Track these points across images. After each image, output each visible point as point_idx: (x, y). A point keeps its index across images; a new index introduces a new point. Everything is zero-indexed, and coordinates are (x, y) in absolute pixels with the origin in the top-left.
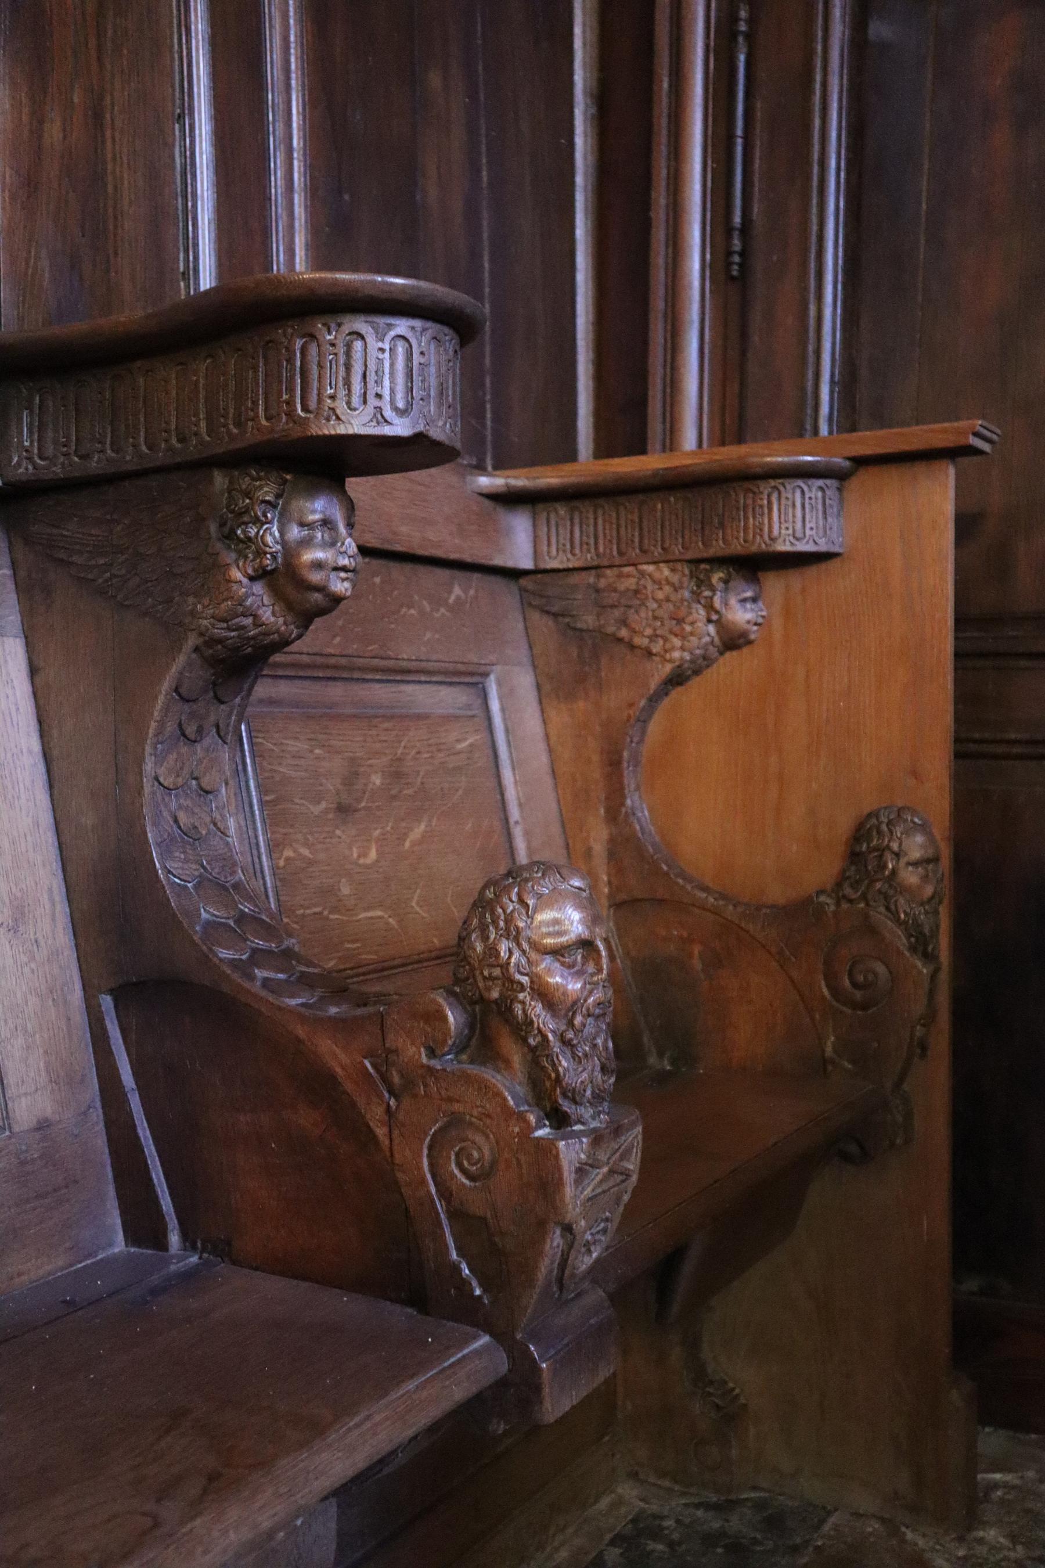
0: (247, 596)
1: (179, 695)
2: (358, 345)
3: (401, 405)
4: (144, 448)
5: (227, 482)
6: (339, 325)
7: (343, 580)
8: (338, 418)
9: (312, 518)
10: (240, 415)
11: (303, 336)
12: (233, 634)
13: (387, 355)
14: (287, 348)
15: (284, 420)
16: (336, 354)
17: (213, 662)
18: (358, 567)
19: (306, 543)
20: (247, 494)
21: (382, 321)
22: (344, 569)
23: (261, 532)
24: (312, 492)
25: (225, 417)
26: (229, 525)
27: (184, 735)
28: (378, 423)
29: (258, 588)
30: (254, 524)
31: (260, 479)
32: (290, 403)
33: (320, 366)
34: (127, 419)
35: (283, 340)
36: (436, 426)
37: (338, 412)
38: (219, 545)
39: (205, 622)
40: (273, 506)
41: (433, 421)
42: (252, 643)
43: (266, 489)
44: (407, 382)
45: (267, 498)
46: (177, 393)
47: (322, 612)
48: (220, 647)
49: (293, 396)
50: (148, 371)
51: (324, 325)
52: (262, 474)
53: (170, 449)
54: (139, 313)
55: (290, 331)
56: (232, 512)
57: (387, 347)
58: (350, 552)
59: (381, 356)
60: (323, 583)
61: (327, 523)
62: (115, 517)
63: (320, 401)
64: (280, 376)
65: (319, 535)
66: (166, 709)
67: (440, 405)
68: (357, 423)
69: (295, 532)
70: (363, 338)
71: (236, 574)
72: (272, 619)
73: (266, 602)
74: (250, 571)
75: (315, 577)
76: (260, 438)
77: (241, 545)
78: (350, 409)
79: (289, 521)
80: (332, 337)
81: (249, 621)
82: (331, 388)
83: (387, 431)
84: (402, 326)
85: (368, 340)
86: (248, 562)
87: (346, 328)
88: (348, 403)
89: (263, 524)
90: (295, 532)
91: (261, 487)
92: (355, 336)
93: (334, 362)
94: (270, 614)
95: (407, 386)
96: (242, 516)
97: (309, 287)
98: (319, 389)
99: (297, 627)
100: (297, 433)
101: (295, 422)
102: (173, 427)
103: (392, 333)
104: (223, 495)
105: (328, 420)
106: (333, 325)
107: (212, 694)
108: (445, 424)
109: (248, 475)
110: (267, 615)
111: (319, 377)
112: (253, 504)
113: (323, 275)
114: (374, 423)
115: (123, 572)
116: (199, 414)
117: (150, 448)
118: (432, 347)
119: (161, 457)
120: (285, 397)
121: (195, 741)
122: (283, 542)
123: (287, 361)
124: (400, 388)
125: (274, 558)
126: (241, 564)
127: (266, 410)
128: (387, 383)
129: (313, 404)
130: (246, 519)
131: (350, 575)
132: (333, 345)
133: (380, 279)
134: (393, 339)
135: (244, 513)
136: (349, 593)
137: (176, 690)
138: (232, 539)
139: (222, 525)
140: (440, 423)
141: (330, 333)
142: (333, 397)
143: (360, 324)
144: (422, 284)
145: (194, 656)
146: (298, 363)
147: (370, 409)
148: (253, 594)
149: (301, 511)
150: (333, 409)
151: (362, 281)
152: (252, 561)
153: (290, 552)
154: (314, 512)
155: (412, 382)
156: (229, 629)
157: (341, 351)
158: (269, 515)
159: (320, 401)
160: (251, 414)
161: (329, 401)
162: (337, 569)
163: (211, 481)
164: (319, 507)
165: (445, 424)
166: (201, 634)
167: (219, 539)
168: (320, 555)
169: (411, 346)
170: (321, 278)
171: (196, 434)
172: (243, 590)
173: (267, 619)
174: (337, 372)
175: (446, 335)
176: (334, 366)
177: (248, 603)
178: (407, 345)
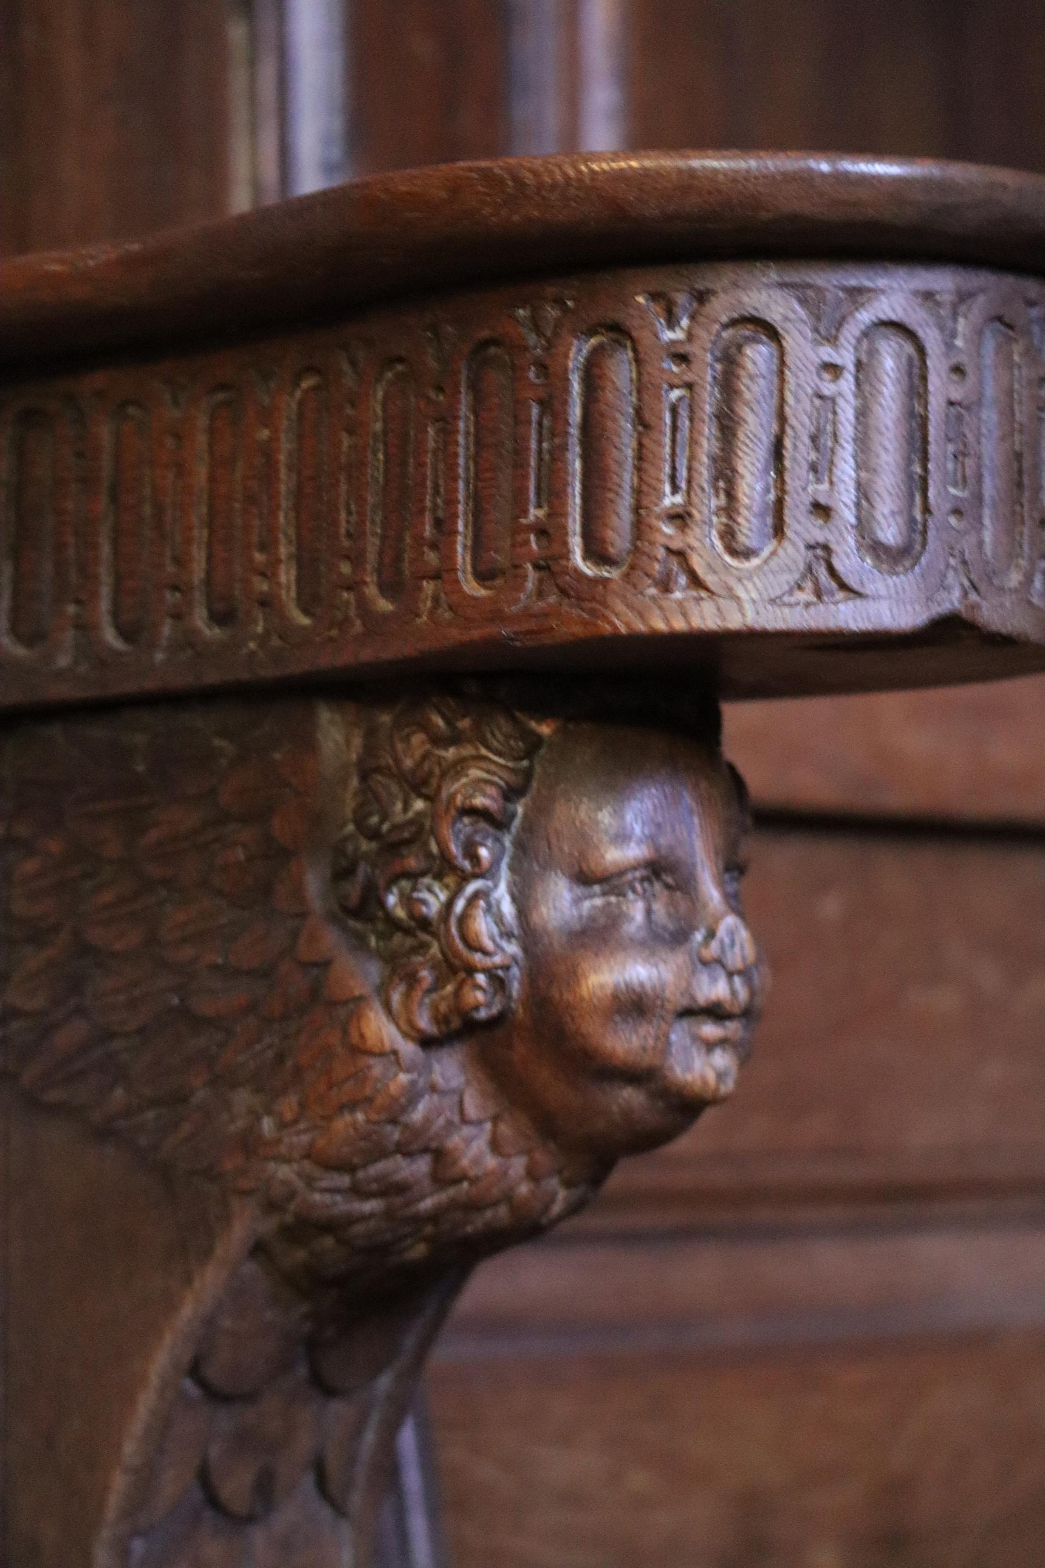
0: (413, 1096)
1: (202, 1383)
2: (758, 356)
3: (890, 533)
4: (110, 636)
5: (357, 742)
6: (701, 297)
7: (710, 1046)
8: (696, 581)
9: (614, 856)
10: (398, 558)
11: (591, 332)
12: (370, 1206)
13: (847, 384)
14: (542, 367)
15: (530, 585)
16: (689, 386)
17: (307, 1283)
18: (759, 1001)
19: (598, 935)
20: (418, 784)
21: (830, 280)
22: (715, 1012)
23: (460, 905)
24: (619, 772)
25: (357, 559)
26: (363, 870)
27: (213, 1501)
28: (818, 593)
29: (449, 1069)
30: (439, 877)
31: (455, 739)
32: (550, 532)
33: (643, 422)
34: (60, 547)
35: (532, 339)
36: (1001, 589)
37: (697, 563)
38: (331, 940)
39: (285, 1172)
40: (497, 822)
41: (989, 577)
42: (429, 1229)
43: (475, 773)
44: (909, 462)
45: (479, 801)
46: (212, 479)
47: (646, 1140)
48: (328, 1242)
49: (557, 513)
50: (125, 404)
51: (655, 296)
52: (464, 724)
53: (188, 640)
54: (97, 255)
55: (552, 313)
56: (374, 835)
57: (846, 358)
58: (734, 960)
59: (828, 388)
60: (647, 1060)
61: (662, 871)
62: (22, 830)
63: (640, 527)
64: (520, 452)
65: (637, 910)
66: (162, 1427)
67: (1012, 521)
68: (754, 595)
69: (561, 903)
70: (773, 334)
71: (380, 1028)
72: (491, 1162)
73: (472, 1110)
74: (424, 1022)
75: (625, 1042)
76: (455, 635)
77: (398, 938)
78: (733, 552)
79: (547, 866)
80: (678, 335)
81: (422, 1165)
82: (675, 489)
83: (847, 616)
84: (895, 292)
85: (788, 343)
86: (418, 994)
87: (721, 308)
88: (728, 535)
89: (465, 878)
90: (561, 903)
91: (459, 767)
92: (746, 331)
93: (684, 413)
94: (482, 1146)
95: (910, 476)
96: (403, 850)
97: (603, 191)
98: (638, 492)
99: (568, 1184)
100: (571, 625)
101: (563, 592)
102: (198, 570)
103: (865, 317)
104: (344, 782)
105: (665, 586)
106: (681, 299)
107: (302, 1371)
108: (1029, 580)
109: (425, 727)
110: (474, 1149)
111: (640, 456)
112: (435, 816)
113: (648, 163)
114: (806, 596)
115: (37, 1002)
116: (276, 542)
117: (127, 634)
118: (989, 345)
119: (161, 665)
120: (535, 514)
121: (250, 1519)
122: (528, 933)
123: (541, 402)
124: (888, 482)
125: (498, 983)
126: (396, 998)
127: (477, 547)
128: (846, 468)
129: (618, 535)
130: (412, 863)
131: (732, 1028)
132: (682, 358)
133: (825, 167)
134: (865, 334)
135: (408, 842)
136: (728, 1086)
137: (195, 1370)
138: (371, 919)
139: (342, 874)
140: (1014, 579)
141: (672, 323)
142: (680, 518)
143: (765, 294)
144: (960, 173)
145: (251, 1268)
146: (576, 413)
147: (793, 553)
148: (433, 1088)
149: (583, 839)
150: (681, 555)
151: (770, 179)
152: (429, 991)
153: (547, 965)
154: (622, 838)
155: (925, 459)
156: (357, 1191)
157: (706, 372)
158: (483, 852)
159: (640, 527)
160: (432, 557)
161: (668, 529)
162: (691, 1012)
163: (307, 743)
164: (631, 822)
165: (1029, 580)
166: (272, 1206)
167: (332, 918)
168: (638, 972)
169: (921, 350)
170: (646, 173)
171: (266, 602)
172: (403, 1078)
173: (476, 1161)
174: (693, 442)
175: (1031, 304)
176: (684, 423)
177: (418, 1114)
178: (909, 349)
